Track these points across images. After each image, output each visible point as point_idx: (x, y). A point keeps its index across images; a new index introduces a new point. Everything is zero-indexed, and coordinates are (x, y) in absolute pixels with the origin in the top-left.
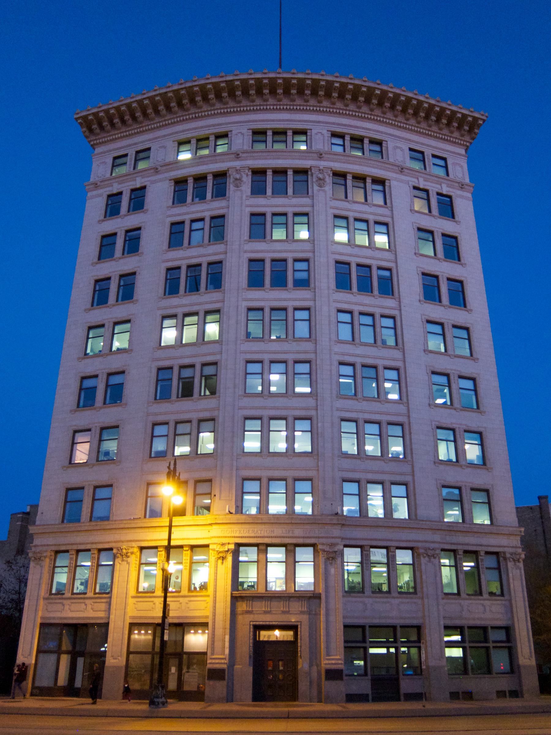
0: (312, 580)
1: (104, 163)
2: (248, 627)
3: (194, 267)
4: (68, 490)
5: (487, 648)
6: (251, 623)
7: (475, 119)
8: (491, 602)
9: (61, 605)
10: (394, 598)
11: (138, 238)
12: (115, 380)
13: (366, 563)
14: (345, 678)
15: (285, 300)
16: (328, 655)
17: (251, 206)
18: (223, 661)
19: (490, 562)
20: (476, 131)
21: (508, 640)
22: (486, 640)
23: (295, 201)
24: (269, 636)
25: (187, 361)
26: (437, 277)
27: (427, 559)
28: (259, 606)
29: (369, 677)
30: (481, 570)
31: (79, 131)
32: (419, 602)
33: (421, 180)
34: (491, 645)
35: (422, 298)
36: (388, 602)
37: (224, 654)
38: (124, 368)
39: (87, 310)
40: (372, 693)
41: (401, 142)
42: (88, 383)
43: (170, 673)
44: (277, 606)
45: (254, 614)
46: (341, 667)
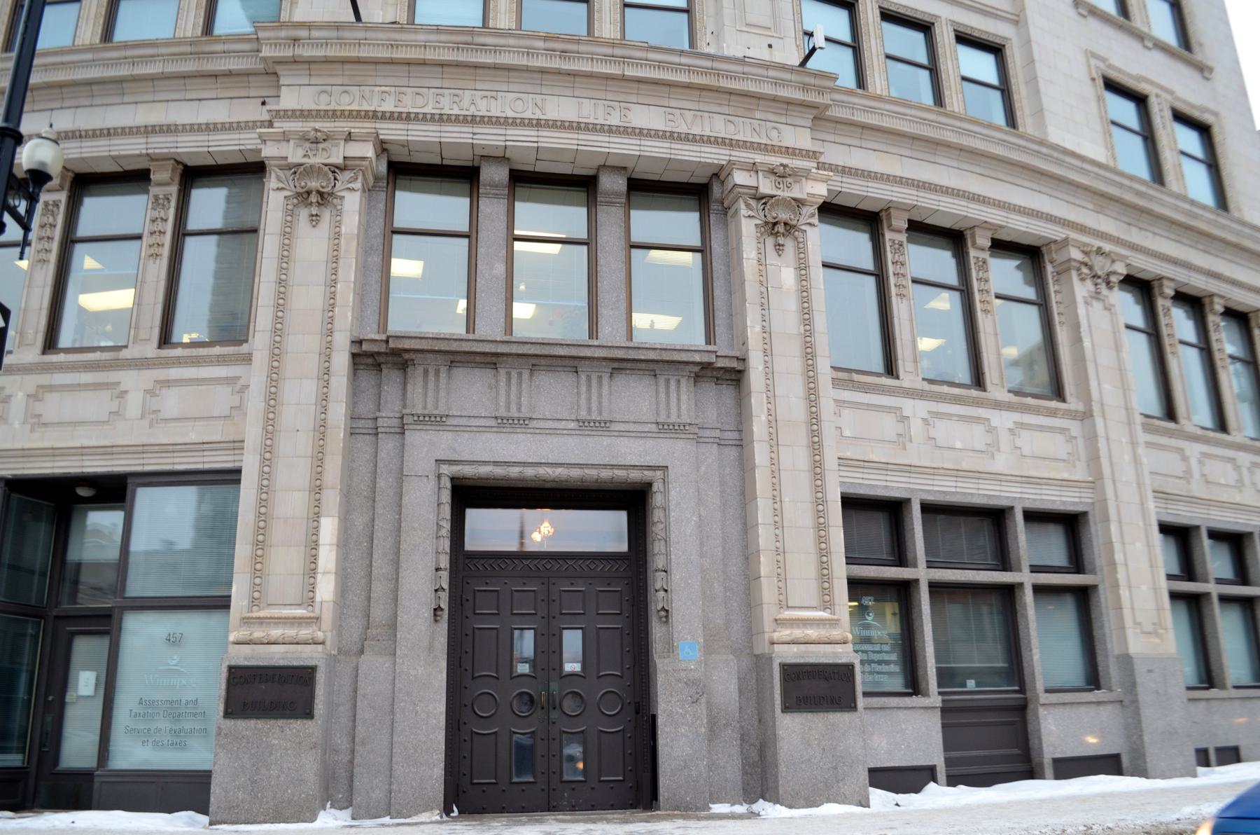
0: (393, 260)
2: (433, 483)
5: (1009, 592)
6: (446, 470)
8: (1017, 417)
9: (1229, 466)
10: (998, 405)
13: (981, 291)
14: (861, 702)
16: (254, 602)
18: (305, 633)
19: (1005, 274)
21: (1077, 562)
22: (1004, 561)
27: (1089, 284)
28: (470, 393)
29: (935, 699)
30: (977, 297)
32: (1074, 427)
34: (1025, 578)
36: (977, 420)
37: (311, 602)
40: (949, 762)
43: (69, 697)
44: (552, 395)
45: (457, 429)
46: (844, 654)
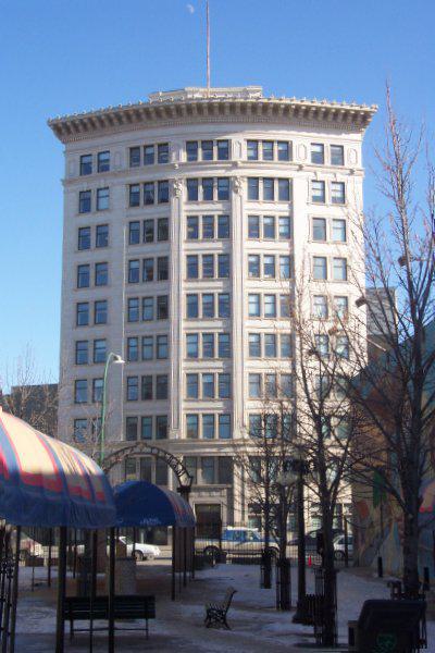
1: (74, 161)
3: (149, 240)
4: (76, 420)
7: (366, 112)
11: (106, 234)
12: (103, 157)
15: (212, 288)
17: (188, 250)
20: (316, 509)
23: (203, 405)
24: (200, 496)
25: (147, 334)
26: (324, 220)
31: (51, 133)
33: (319, 173)
35: (311, 239)
38: (107, 260)
39: (77, 215)
41: (303, 141)
42: (85, 160)
